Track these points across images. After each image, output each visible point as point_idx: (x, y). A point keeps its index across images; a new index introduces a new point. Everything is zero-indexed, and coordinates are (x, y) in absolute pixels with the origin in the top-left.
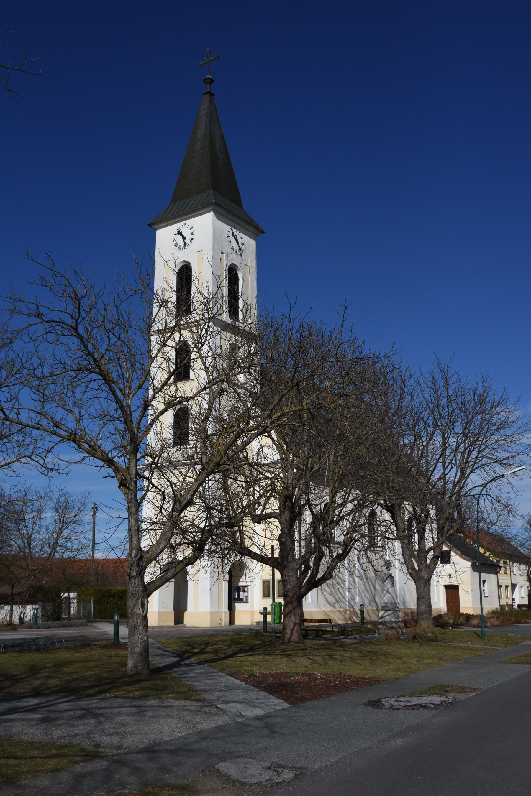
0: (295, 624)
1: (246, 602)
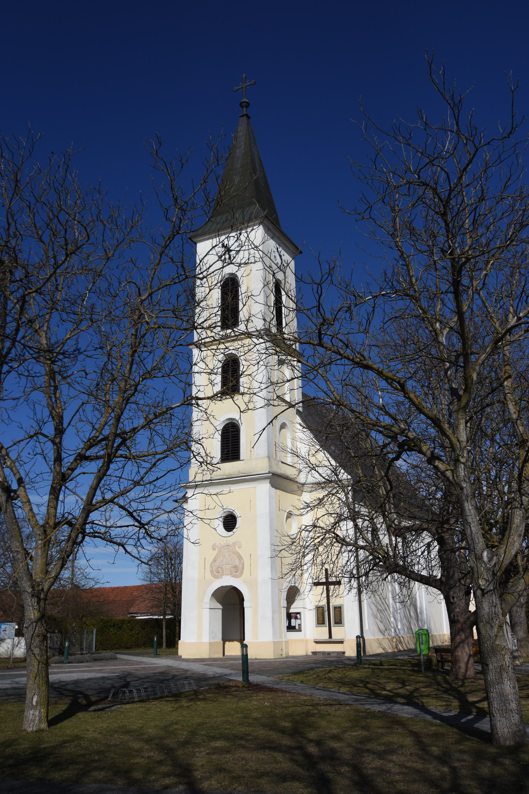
0: (470, 656)
1: (300, 630)
